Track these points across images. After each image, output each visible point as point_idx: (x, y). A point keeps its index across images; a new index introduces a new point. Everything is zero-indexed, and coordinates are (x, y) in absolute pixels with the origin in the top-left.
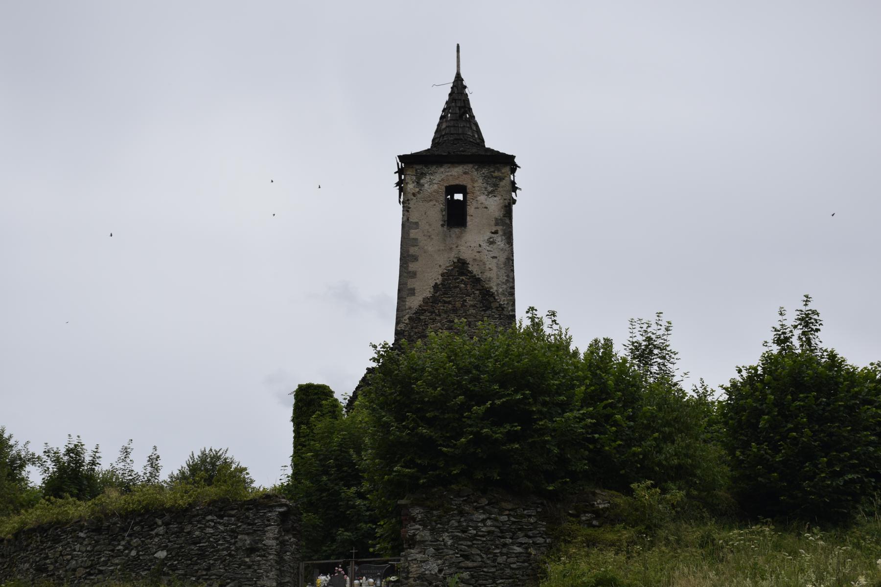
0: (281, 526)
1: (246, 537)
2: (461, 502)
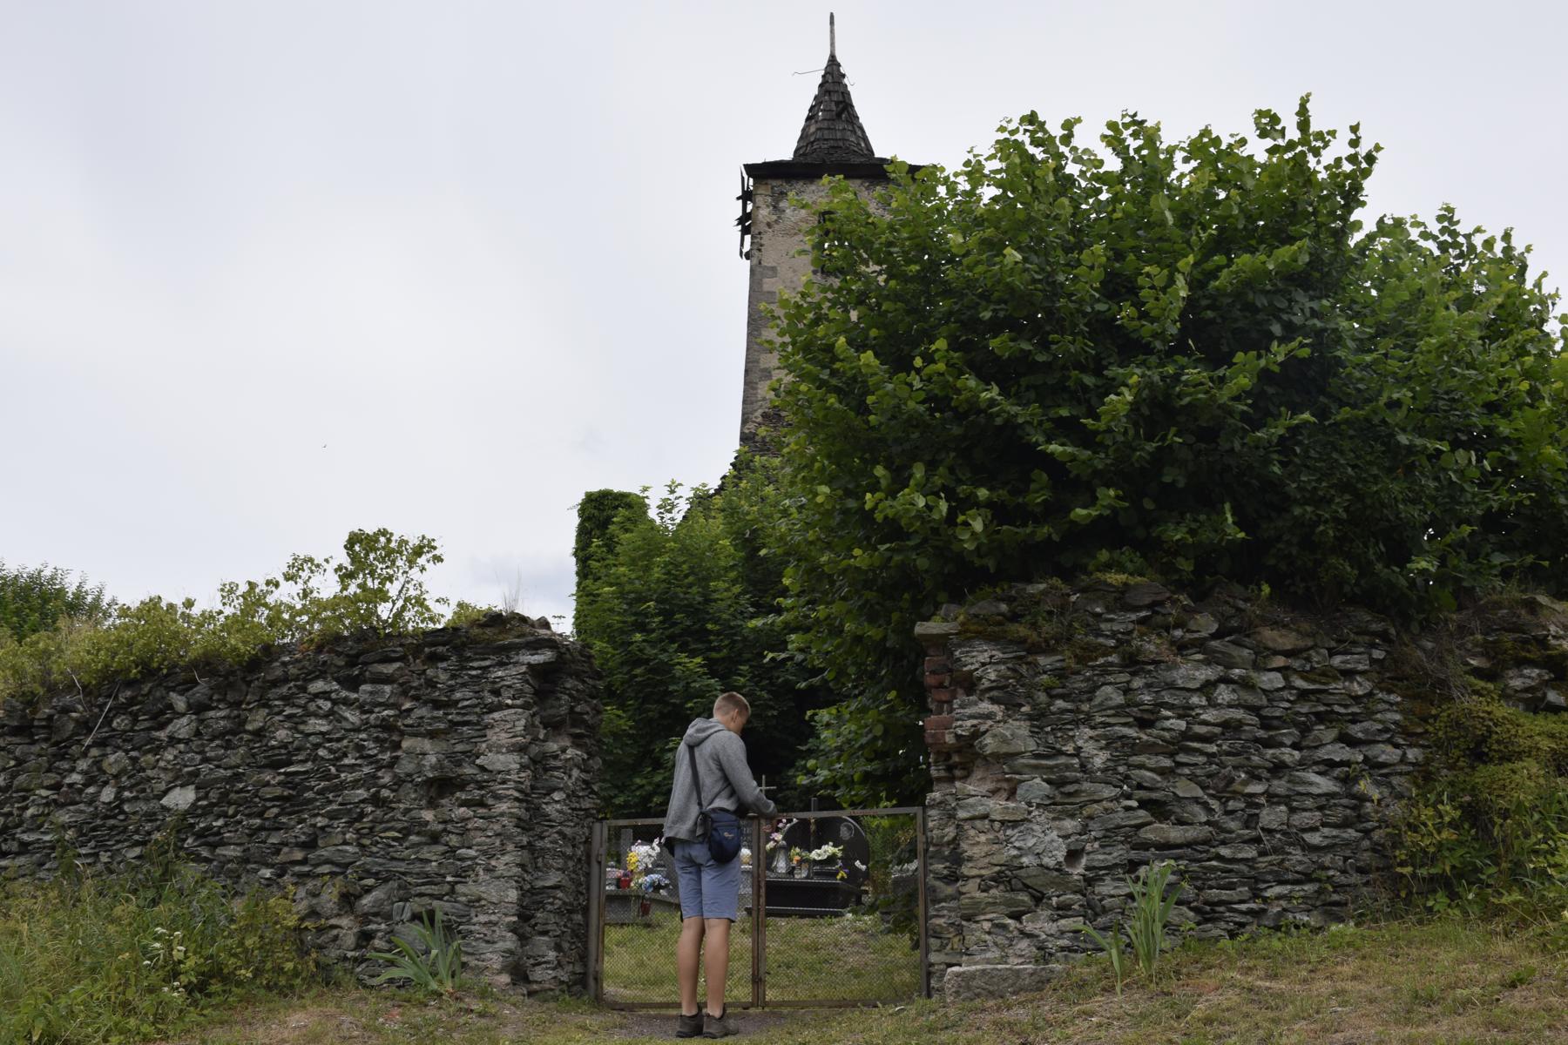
0: (535, 709)
1: (427, 745)
2: (1131, 626)
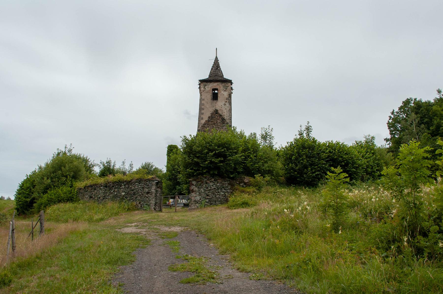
1: (146, 189)
